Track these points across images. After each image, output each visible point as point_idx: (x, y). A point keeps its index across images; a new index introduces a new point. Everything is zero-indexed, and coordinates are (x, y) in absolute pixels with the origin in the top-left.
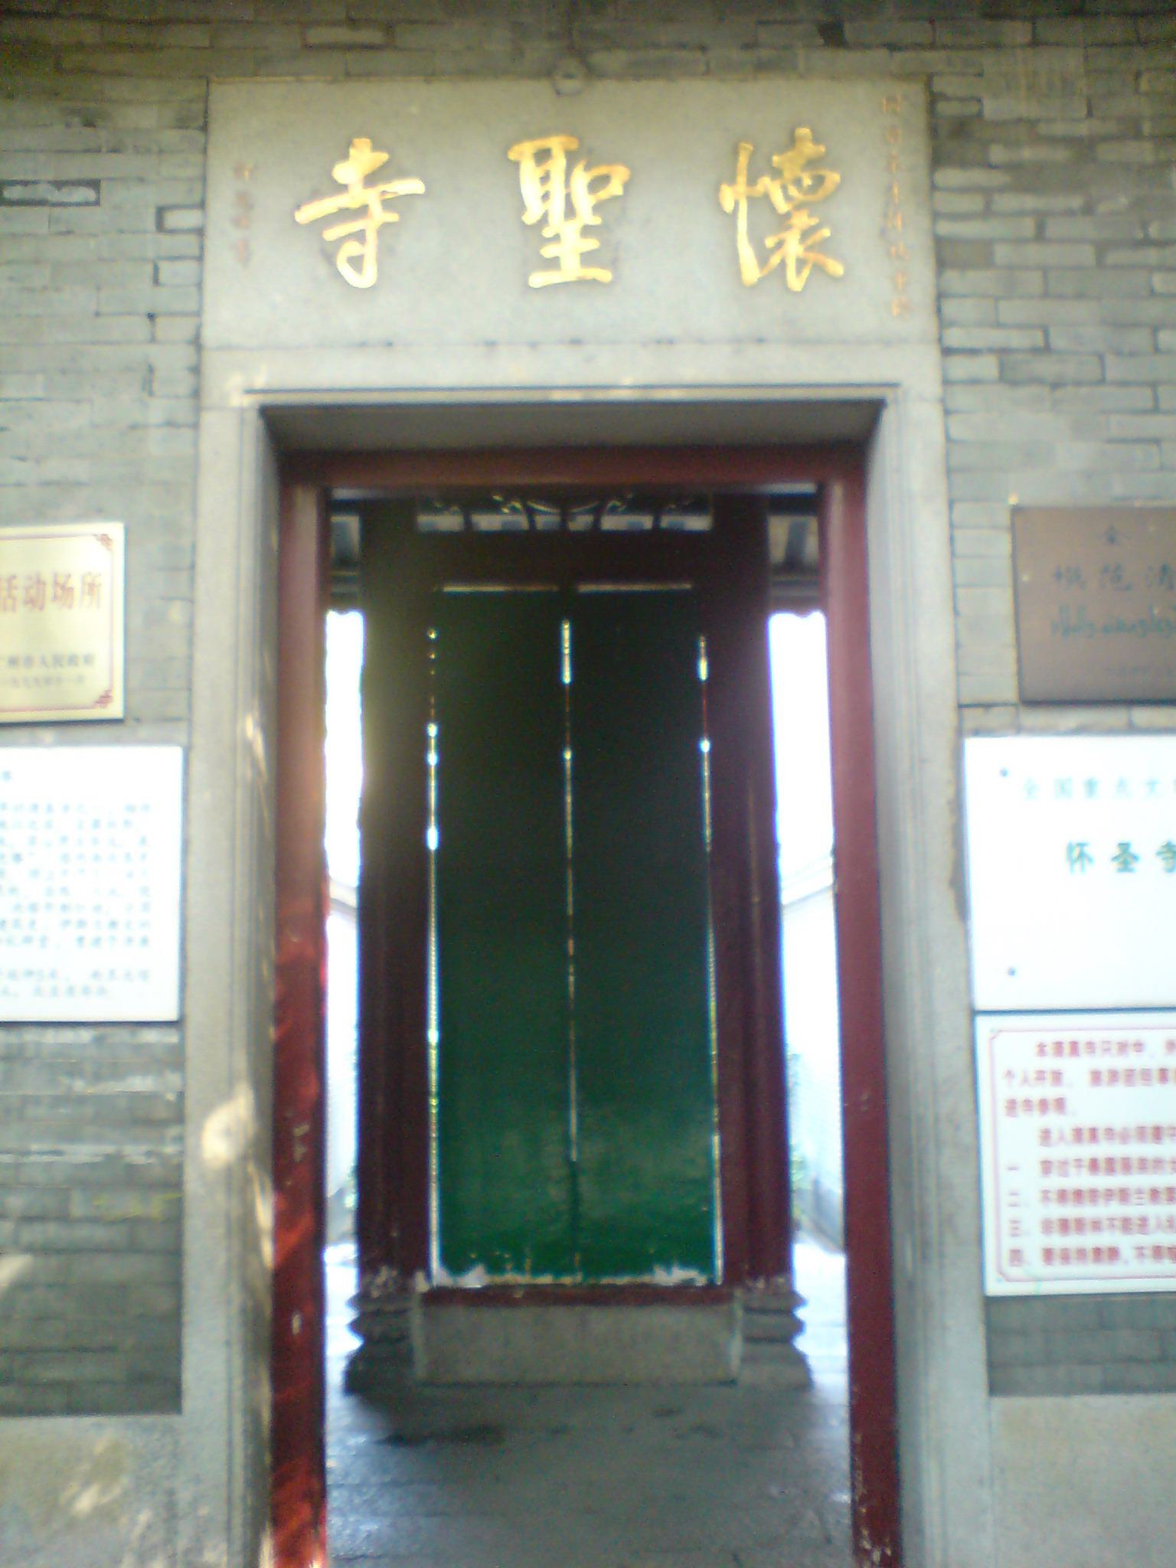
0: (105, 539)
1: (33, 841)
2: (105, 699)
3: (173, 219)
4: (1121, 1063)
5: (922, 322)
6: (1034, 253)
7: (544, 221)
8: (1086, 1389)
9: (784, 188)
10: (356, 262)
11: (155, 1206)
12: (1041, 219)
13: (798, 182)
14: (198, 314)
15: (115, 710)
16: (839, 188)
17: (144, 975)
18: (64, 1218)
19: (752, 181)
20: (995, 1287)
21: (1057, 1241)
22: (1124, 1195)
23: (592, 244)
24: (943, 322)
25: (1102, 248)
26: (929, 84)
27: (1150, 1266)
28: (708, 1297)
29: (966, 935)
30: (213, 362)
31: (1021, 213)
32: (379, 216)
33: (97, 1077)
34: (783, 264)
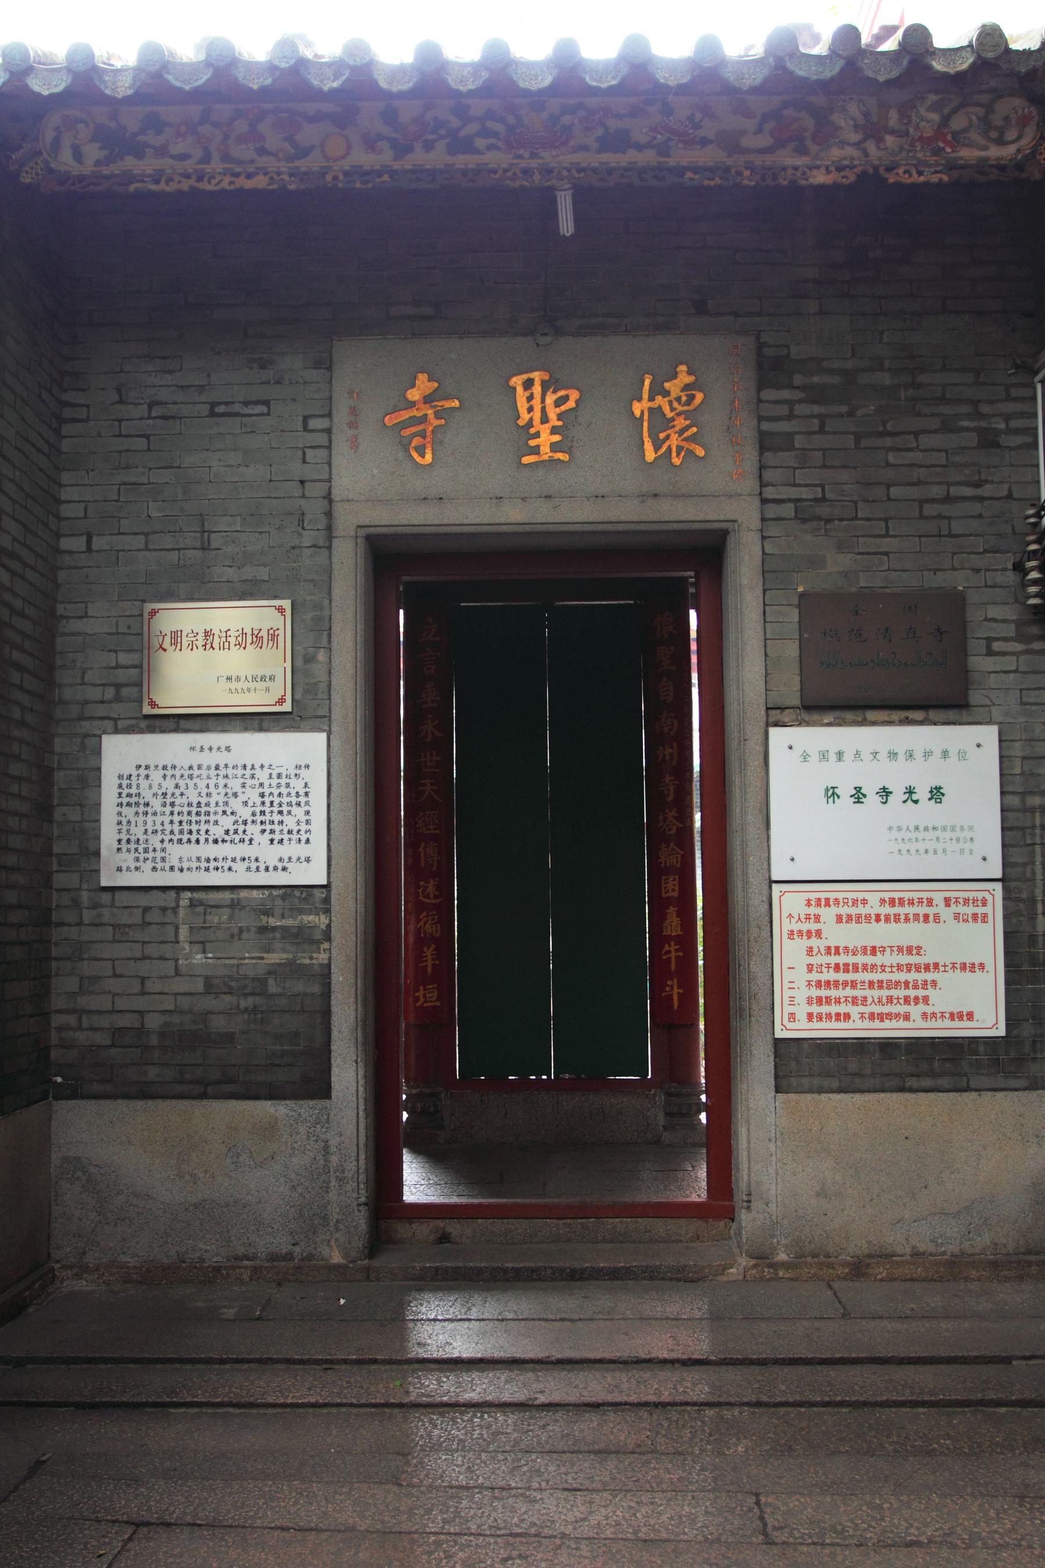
1: (243, 786)
3: (313, 424)
4: (853, 911)
5: (750, 484)
6: (820, 440)
7: (530, 424)
8: (831, 1091)
9: (670, 403)
12: (822, 418)
14: (329, 480)
17: (308, 860)
20: (779, 1034)
21: (815, 1009)
22: (853, 984)
23: (557, 438)
24: (763, 485)
25: (858, 437)
26: (758, 338)
27: (867, 1024)
30: (339, 509)
31: (811, 416)
34: (669, 448)
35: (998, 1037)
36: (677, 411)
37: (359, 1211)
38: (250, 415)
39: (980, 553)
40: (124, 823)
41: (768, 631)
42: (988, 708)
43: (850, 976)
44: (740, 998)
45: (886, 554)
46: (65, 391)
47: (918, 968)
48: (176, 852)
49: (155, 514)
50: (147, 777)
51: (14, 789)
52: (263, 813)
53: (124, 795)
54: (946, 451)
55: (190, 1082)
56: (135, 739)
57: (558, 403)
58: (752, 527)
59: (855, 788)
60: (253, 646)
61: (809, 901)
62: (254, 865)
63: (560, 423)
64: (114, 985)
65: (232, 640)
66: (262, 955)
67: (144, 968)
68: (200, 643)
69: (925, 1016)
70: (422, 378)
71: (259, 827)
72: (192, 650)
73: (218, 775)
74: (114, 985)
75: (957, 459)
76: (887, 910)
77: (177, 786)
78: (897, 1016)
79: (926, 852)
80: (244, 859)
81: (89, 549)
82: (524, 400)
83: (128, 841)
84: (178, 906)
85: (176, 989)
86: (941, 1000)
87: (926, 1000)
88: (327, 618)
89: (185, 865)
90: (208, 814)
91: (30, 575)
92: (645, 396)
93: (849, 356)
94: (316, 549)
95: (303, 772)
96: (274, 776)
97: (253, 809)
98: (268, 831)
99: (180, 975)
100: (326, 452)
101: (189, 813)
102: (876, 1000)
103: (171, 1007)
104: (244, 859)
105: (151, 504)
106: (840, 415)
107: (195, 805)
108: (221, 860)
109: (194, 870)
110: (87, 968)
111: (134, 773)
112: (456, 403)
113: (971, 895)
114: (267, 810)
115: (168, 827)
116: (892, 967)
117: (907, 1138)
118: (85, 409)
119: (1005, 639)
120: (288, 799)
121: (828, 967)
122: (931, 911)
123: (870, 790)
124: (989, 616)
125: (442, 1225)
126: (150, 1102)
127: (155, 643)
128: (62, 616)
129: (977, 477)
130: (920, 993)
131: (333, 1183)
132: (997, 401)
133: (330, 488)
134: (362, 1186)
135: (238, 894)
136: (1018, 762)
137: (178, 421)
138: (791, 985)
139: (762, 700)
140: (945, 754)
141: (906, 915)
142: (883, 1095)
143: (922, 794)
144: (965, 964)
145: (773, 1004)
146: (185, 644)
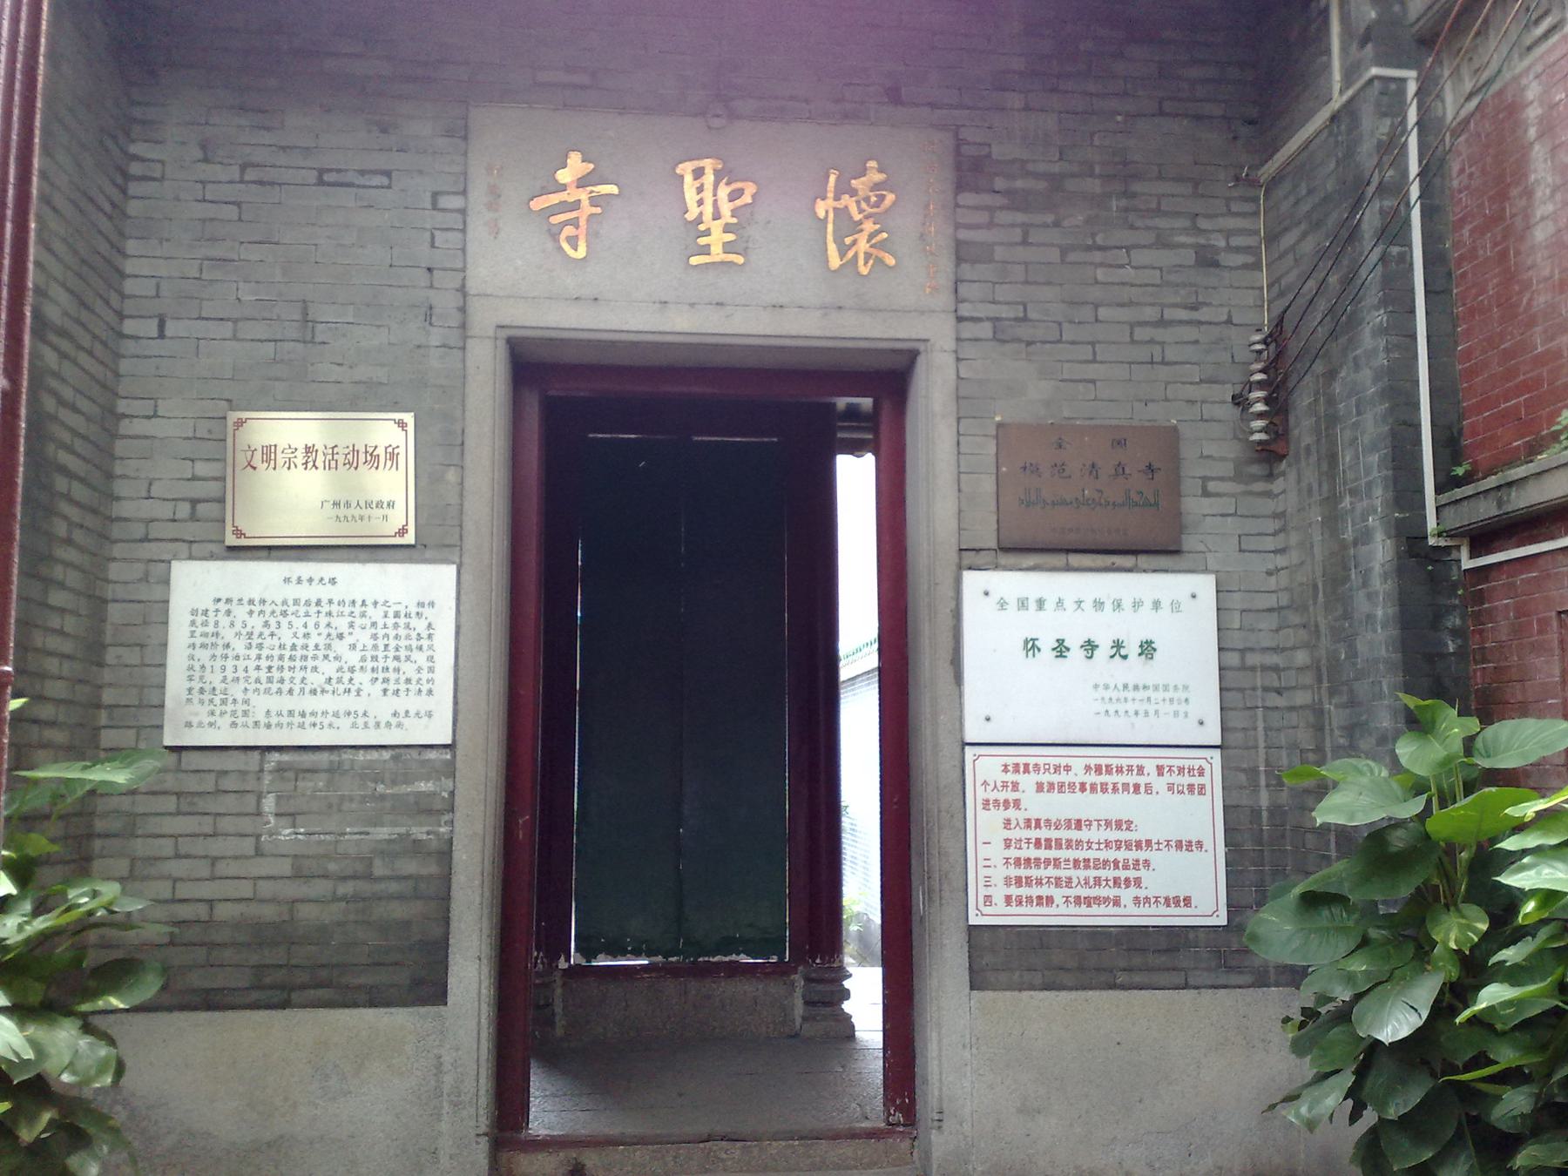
0: (402, 424)
1: (351, 625)
2: (402, 532)
3: (444, 202)
4: (1055, 778)
5: (945, 299)
6: (1022, 253)
7: (699, 220)
8: (1032, 988)
9: (858, 203)
10: (574, 245)
11: (432, 869)
12: (1026, 228)
13: (867, 200)
14: (464, 270)
15: (410, 538)
16: (894, 203)
17: (429, 715)
18: (369, 877)
19: (837, 198)
20: (974, 920)
21: (1014, 891)
22: (1057, 863)
23: (730, 237)
24: (959, 300)
25: (1064, 251)
26: (956, 134)
27: (1073, 909)
28: (782, 970)
29: (961, 695)
30: (475, 306)
31: (1013, 225)
32: (587, 209)
33: (394, 783)
34: (856, 256)
35: (1219, 927)
36: (865, 213)
37: (477, 1143)
38: (364, 187)
39: (1197, 383)
40: (197, 668)
41: (962, 464)
42: (1203, 555)
43: (1052, 854)
44: (929, 878)
45: (1093, 382)
46: (133, 141)
47: (1128, 846)
48: (262, 704)
49: (246, 298)
50: (228, 612)
51: (55, 622)
52: (375, 658)
53: (197, 634)
54: (1161, 269)
55: (271, 987)
56: (215, 567)
57: (733, 197)
58: (946, 348)
59: (1058, 640)
60: (367, 466)
61: (1006, 766)
62: (360, 721)
63: (735, 220)
64: (177, 868)
65: (341, 458)
66: (366, 829)
67: (216, 847)
68: (300, 460)
69: (1137, 900)
70: (575, 159)
71: (369, 675)
72: (289, 468)
73: (319, 612)
74: (177, 868)
75: (1173, 278)
76: (1092, 778)
77: (266, 624)
78: (1106, 900)
79: (1136, 713)
80: (349, 714)
81: (162, 336)
82: (694, 191)
83: (202, 691)
84: (262, 770)
85: (255, 872)
86: (1154, 883)
87: (1138, 882)
88: (460, 432)
89: (274, 720)
90: (305, 658)
91: (83, 358)
92: (830, 195)
93: (1057, 158)
94: (446, 350)
95: (427, 611)
96: (391, 614)
97: (363, 653)
98: (381, 680)
99: (262, 855)
100: (459, 235)
101: (281, 658)
102: (1083, 882)
103: (249, 894)
104: (349, 714)
105: (241, 285)
106: (1045, 226)
107: (288, 647)
108: (319, 714)
109: (285, 726)
110: (140, 847)
111: (212, 608)
112: (612, 189)
113: (1187, 763)
114: (381, 655)
115: (253, 674)
116: (1099, 843)
117: (1119, 1044)
118: (159, 166)
119: (1221, 479)
120: (408, 643)
121: (1028, 843)
122: (1142, 780)
123: (1074, 643)
124: (1205, 454)
125: (574, 1156)
126: (217, 1015)
127: (241, 459)
128: (124, 416)
129: (1193, 299)
130: (1132, 874)
131: (446, 1107)
132: (1216, 216)
133: (464, 279)
134: (481, 1112)
135: (340, 756)
136: (1237, 615)
137: (277, 188)
138: (988, 863)
139: (954, 540)
140: (1157, 605)
141: (1115, 785)
142: (1091, 993)
143: (1132, 649)
144: (1181, 841)
145: (967, 885)
146: (280, 462)
